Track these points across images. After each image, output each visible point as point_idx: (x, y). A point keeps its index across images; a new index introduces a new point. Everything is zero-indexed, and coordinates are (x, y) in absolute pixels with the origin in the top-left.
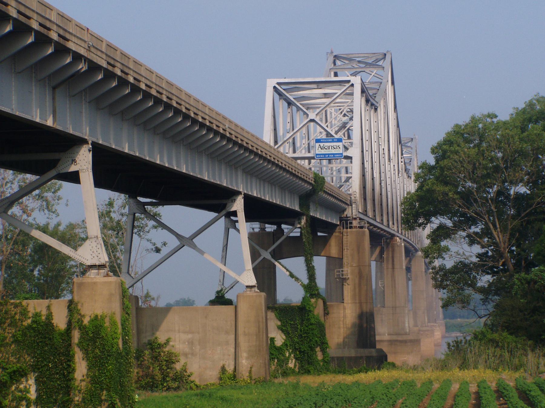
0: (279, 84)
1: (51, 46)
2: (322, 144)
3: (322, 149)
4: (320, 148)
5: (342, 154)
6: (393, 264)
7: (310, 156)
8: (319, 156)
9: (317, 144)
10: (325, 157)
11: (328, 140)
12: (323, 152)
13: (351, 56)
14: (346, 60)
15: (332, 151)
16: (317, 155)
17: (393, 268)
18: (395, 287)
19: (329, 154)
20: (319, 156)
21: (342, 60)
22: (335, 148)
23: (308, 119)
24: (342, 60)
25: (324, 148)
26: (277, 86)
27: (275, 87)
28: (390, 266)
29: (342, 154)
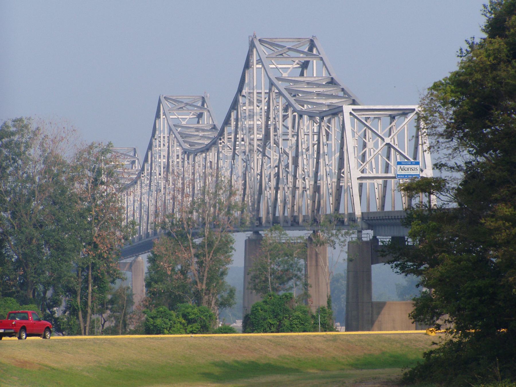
0: (353, 110)
1: (479, 153)
2: (402, 166)
3: (402, 170)
4: (400, 170)
5: (419, 175)
6: (317, 261)
7: (392, 176)
8: (400, 176)
9: (399, 166)
10: (405, 177)
11: (407, 163)
12: (403, 173)
13: (274, 40)
14: (266, 44)
15: (410, 172)
16: (398, 175)
17: (317, 265)
18: (319, 285)
19: (408, 175)
20: (400, 176)
21: (263, 44)
22: (413, 170)
23: (385, 143)
24: (263, 44)
25: (404, 169)
26: (353, 112)
27: (351, 113)
28: (314, 263)
29: (419, 175)
